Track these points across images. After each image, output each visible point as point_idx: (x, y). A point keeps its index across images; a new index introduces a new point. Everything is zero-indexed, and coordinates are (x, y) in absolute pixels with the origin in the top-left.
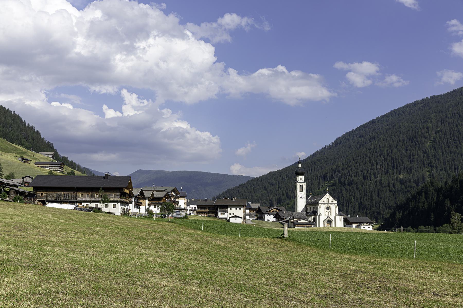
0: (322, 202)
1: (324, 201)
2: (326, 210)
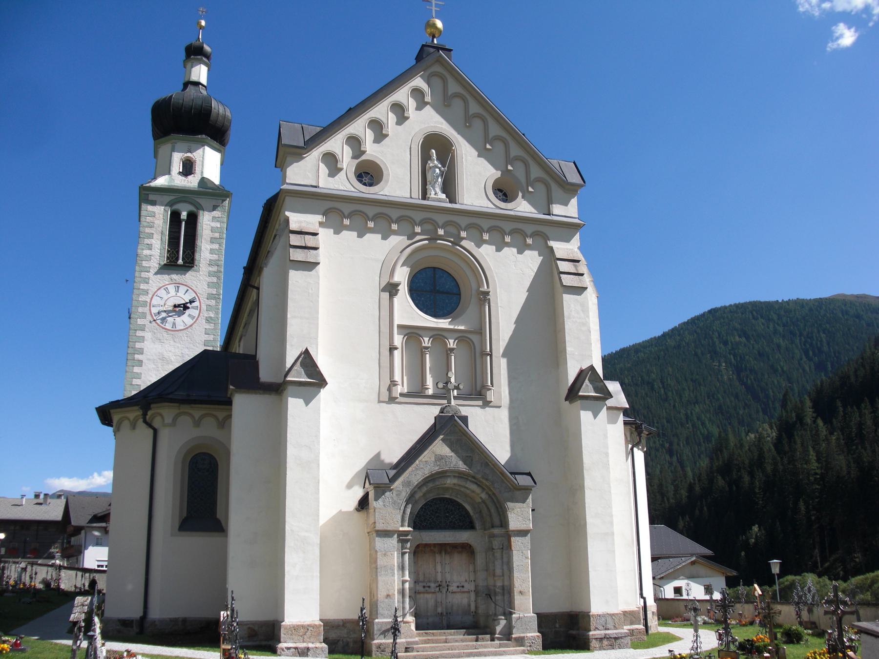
0: (344, 184)
1: (369, 174)
2: (407, 311)
